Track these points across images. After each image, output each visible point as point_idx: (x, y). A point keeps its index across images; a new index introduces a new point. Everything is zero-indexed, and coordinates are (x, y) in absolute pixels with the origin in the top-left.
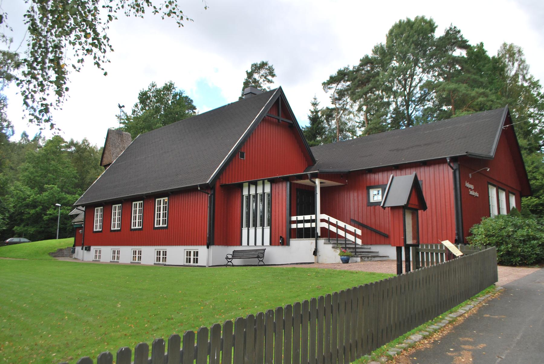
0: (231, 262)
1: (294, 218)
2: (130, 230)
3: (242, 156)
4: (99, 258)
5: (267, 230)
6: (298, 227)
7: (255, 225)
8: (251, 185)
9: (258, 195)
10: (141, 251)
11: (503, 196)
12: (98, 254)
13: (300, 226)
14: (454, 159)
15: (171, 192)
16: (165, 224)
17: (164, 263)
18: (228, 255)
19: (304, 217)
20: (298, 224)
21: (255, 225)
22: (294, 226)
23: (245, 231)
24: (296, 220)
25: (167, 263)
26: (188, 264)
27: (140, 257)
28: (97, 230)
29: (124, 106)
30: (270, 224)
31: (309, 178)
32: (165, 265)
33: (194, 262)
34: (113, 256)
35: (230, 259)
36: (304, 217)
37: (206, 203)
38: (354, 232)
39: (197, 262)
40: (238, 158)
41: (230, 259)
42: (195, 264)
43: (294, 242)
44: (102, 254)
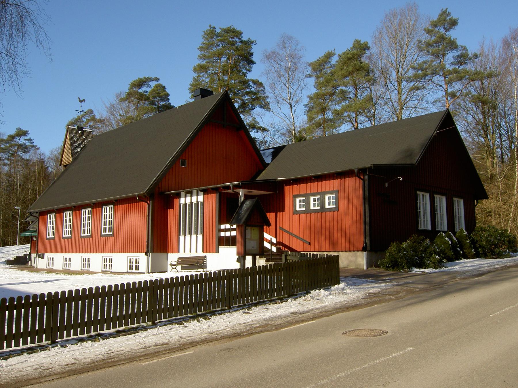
0: (175, 268)
1: (223, 227)
2: (294, 214)
3: (183, 164)
4: (69, 267)
5: (200, 237)
6: (232, 235)
7: (191, 234)
8: (187, 194)
9: (199, 203)
10: (112, 259)
11: (441, 201)
12: (51, 262)
13: (228, 234)
14: (362, 172)
15: (115, 200)
16: (111, 232)
17: (110, 270)
18: (172, 262)
19: (225, 226)
20: (226, 232)
21: (191, 234)
22: (222, 234)
23: (182, 237)
24: (224, 228)
25: (113, 270)
26: (131, 271)
27: (138, 266)
28: (65, 236)
29: (84, 100)
30: (202, 233)
31: (232, 189)
32: (111, 272)
33: (136, 269)
34: (130, 265)
35: (174, 265)
36: (225, 226)
37: (146, 212)
38: (270, 240)
39: (138, 269)
40: (179, 167)
41: (174, 265)
42: (137, 271)
43: (222, 249)
44: (55, 262)
